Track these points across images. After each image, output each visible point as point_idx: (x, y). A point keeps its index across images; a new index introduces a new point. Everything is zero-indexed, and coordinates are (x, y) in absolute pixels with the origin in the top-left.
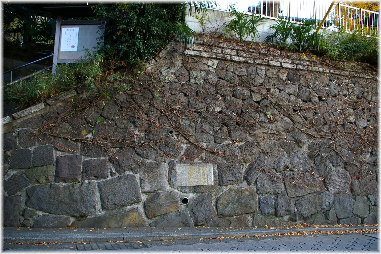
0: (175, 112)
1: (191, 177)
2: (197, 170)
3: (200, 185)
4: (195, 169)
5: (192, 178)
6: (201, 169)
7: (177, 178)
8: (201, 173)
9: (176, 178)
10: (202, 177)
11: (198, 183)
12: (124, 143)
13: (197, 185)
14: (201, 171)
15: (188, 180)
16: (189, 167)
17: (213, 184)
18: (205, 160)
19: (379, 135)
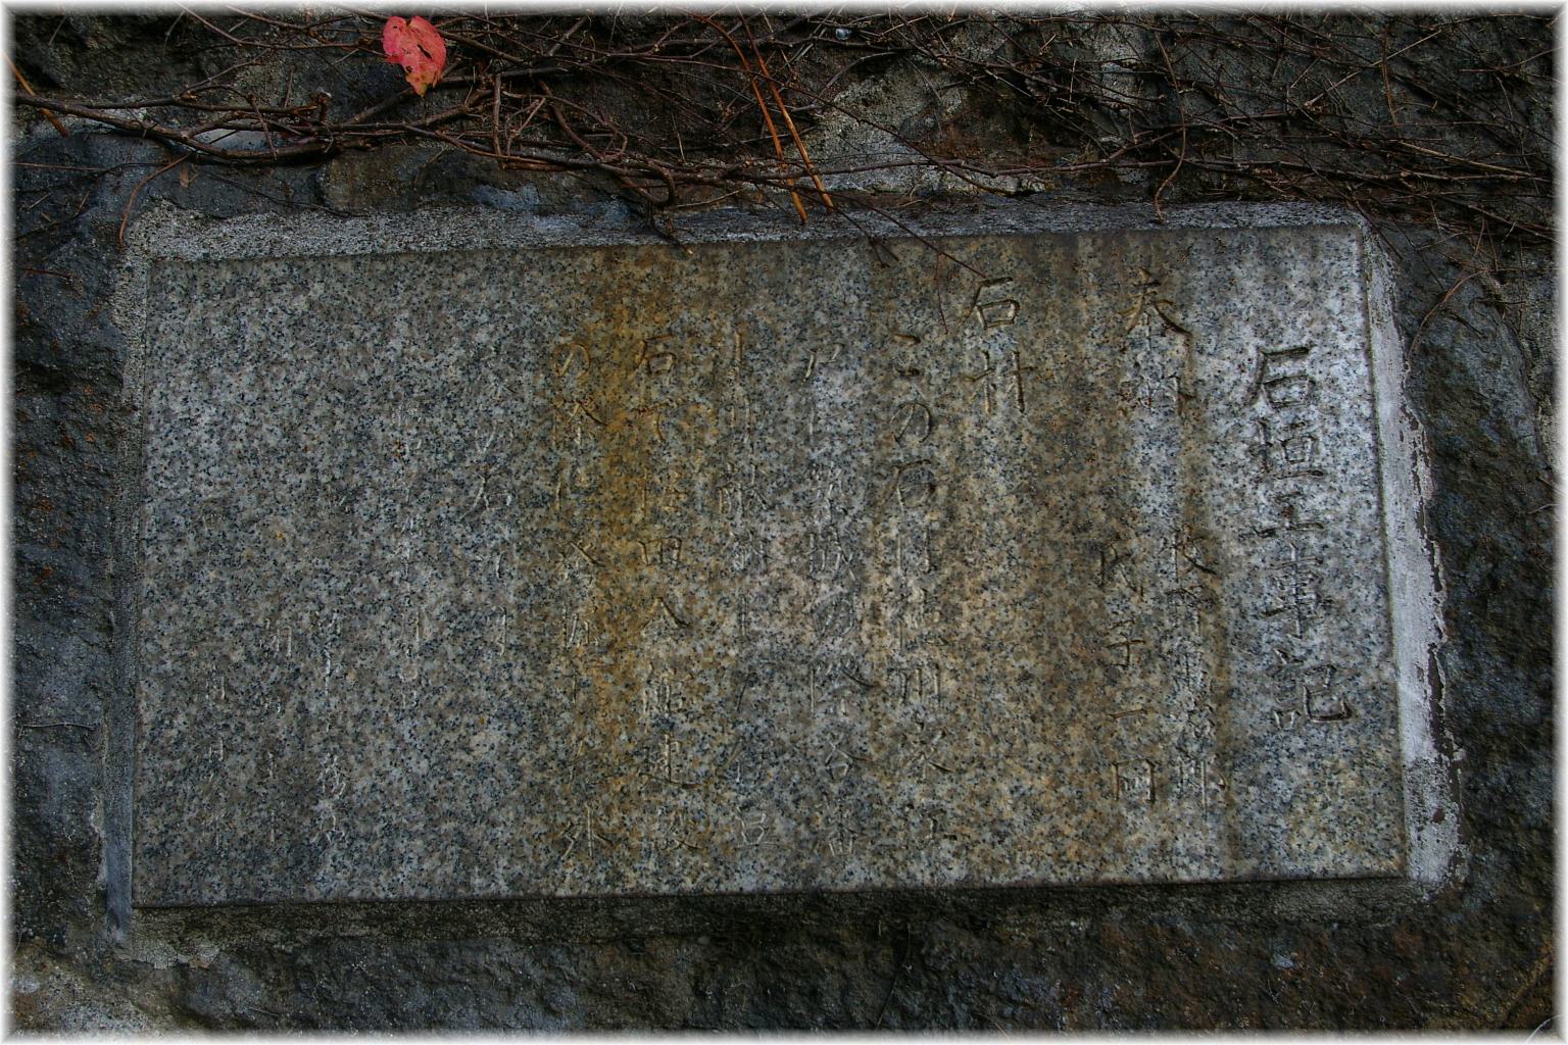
0: (351, 678)
1: (620, 618)
2: (835, 389)
3: (943, 867)
4: (757, 342)
5: (657, 646)
6: (983, 373)
7: (161, 632)
8: (994, 485)
9: (113, 629)
10: (989, 610)
11: (866, 823)
12: (319, 199)
13: (857, 872)
14: (993, 421)
15: (531, 720)
16: (545, 297)
17: (1432, 857)
18: (1063, 28)
19: (1137, 9)
